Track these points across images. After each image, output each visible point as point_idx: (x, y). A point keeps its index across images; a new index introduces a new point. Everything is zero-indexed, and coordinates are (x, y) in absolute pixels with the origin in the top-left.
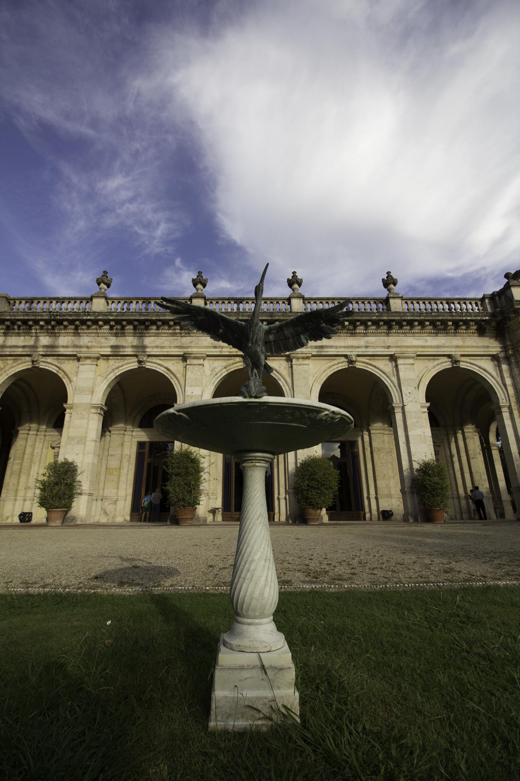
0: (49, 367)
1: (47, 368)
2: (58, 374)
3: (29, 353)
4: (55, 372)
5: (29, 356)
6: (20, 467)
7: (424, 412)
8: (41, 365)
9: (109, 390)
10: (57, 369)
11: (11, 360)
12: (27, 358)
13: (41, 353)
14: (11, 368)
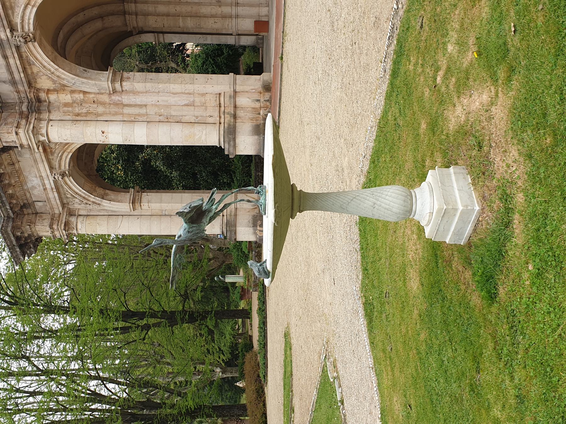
0: (29, 19)
1: (31, 21)
2: (38, 4)
3: (14, 49)
4: (35, 9)
5: (18, 48)
6: (189, 18)
7: (231, 132)
8: (29, 30)
9: (186, 191)
10: (30, 7)
11: (31, 69)
12: (24, 49)
13: (9, 34)
14: (44, 67)
